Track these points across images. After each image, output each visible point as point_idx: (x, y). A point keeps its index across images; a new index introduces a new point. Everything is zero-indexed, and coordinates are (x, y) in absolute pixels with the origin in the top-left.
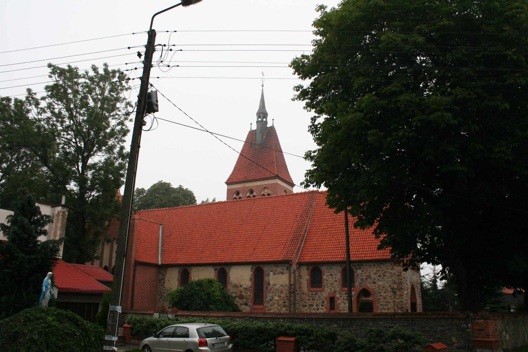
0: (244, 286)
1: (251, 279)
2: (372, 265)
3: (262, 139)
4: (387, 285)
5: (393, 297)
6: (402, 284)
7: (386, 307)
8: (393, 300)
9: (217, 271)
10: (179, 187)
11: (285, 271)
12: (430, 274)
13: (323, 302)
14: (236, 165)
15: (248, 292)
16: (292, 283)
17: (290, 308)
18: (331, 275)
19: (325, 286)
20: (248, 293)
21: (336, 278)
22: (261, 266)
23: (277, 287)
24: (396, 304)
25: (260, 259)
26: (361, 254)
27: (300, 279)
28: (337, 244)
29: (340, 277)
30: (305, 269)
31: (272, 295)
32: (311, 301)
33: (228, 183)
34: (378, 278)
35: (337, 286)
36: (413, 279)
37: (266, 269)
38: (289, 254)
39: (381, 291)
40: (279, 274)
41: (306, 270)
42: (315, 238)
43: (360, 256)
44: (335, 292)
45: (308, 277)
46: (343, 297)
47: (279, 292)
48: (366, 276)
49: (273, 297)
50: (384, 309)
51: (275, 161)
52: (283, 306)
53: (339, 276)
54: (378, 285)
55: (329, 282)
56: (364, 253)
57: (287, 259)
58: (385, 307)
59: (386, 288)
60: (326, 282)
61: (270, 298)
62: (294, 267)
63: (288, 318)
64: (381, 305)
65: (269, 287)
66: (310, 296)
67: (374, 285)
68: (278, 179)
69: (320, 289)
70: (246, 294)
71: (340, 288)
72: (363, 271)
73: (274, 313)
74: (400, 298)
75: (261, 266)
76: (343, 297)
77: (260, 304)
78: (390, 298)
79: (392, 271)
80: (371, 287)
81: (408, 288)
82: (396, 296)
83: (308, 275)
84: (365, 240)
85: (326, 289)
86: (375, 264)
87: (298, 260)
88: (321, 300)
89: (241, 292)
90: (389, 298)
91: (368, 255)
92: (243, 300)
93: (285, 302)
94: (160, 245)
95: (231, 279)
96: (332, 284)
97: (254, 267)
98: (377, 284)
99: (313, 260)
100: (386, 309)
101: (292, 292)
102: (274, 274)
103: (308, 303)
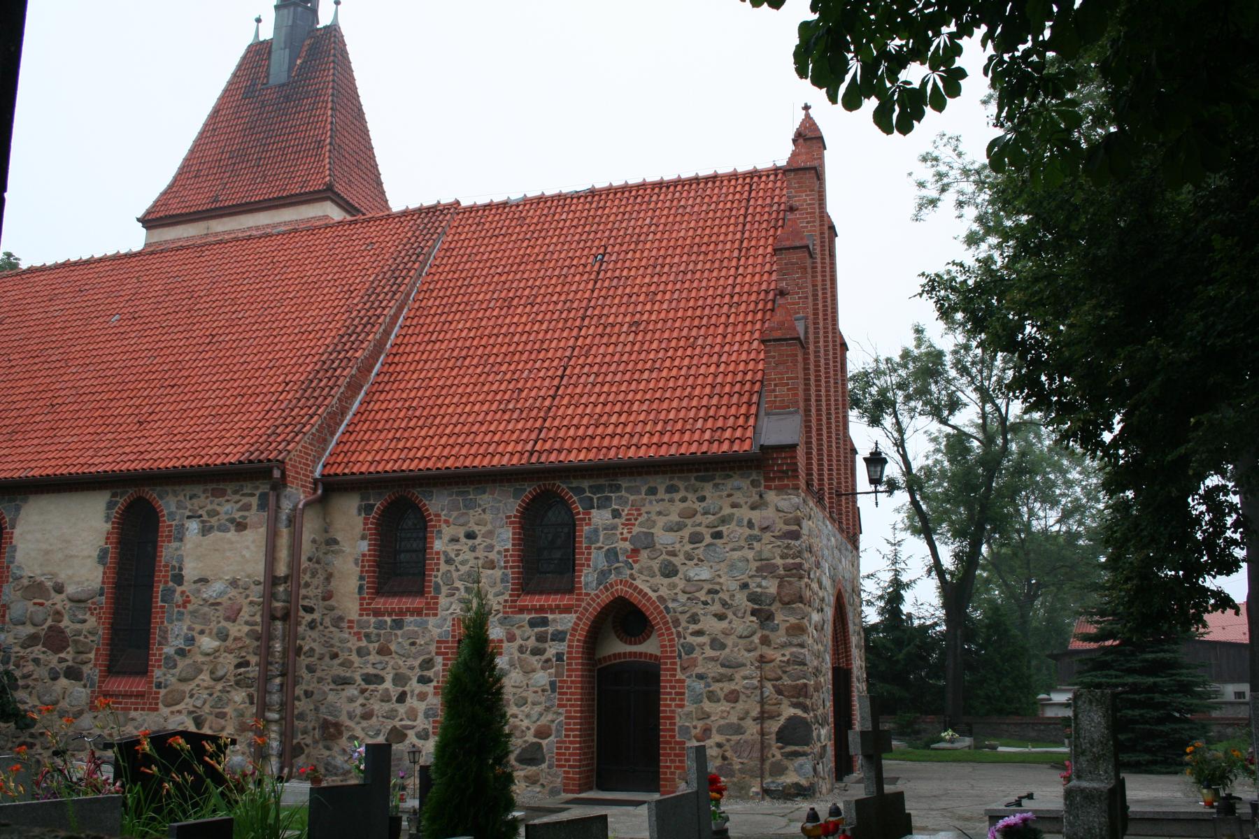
0: (70, 590)
1: (102, 558)
2: (661, 483)
3: (290, 69)
5: (756, 639)
6: (801, 577)
7: (721, 688)
8: (756, 654)
11: (254, 516)
12: (878, 575)
13: (427, 664)
14: (186, 160)
15: (87, 616)
16: (282, 570)
18: (470, 536)
19: (438, 589)
20: (84, 621)
21: (490, 548)
23: (211, 591)
24: (773, 675)
26: (612, 436)
27: (330, 556)
28: (507, 397)
29: (509, 546)
30: (354, 511)
31: (190, 629)
32: (373, 658)
34: (688, 547)
36: (840, 567)
39: (699, 609)
40: (227, 530)
43: (606, 442)
45: (364, 546)
46: (519, 642)
47: (221, 613)
48: (632, 540)
49: (193, 639)
51: (328, 140)
52: (238, 683)
53: (506, 538)
54: (689, 580)
55: (458, 570)
56: (628, 429)
58: (716, 687)
59: (726, 596)
60: (444, 567)
61: (180, 643)
62: (297, 495)
64: (700, 677)
65: (179, 589)
66: (367, 636)
67: (666, 581)
68: (333, 201)
69: (417, 602)
70: (78, 626)
71: (507, 597)
72: (616, 514)
74: (791, 644)
75: (152, 494)
76: (519, 642)
77: (137, 673)
78: (742, 641)
79: (756, 515)
80: (655, 591)
82: (772, 636)
83: (363, 538)
84: (636, 376)
85: (443, 601)
86: (675, 482)
87: (324, 466)
88: (420, 653)
89: (58, 614)
90: (736, 645)
91: (645, 440)
92: (62, 655)
93: (247, 664)
95: (19, 556)
97: (121, 501)
98: (680, 575)
101: (279, 614)
102: (206, 530)
103: (361, 667)
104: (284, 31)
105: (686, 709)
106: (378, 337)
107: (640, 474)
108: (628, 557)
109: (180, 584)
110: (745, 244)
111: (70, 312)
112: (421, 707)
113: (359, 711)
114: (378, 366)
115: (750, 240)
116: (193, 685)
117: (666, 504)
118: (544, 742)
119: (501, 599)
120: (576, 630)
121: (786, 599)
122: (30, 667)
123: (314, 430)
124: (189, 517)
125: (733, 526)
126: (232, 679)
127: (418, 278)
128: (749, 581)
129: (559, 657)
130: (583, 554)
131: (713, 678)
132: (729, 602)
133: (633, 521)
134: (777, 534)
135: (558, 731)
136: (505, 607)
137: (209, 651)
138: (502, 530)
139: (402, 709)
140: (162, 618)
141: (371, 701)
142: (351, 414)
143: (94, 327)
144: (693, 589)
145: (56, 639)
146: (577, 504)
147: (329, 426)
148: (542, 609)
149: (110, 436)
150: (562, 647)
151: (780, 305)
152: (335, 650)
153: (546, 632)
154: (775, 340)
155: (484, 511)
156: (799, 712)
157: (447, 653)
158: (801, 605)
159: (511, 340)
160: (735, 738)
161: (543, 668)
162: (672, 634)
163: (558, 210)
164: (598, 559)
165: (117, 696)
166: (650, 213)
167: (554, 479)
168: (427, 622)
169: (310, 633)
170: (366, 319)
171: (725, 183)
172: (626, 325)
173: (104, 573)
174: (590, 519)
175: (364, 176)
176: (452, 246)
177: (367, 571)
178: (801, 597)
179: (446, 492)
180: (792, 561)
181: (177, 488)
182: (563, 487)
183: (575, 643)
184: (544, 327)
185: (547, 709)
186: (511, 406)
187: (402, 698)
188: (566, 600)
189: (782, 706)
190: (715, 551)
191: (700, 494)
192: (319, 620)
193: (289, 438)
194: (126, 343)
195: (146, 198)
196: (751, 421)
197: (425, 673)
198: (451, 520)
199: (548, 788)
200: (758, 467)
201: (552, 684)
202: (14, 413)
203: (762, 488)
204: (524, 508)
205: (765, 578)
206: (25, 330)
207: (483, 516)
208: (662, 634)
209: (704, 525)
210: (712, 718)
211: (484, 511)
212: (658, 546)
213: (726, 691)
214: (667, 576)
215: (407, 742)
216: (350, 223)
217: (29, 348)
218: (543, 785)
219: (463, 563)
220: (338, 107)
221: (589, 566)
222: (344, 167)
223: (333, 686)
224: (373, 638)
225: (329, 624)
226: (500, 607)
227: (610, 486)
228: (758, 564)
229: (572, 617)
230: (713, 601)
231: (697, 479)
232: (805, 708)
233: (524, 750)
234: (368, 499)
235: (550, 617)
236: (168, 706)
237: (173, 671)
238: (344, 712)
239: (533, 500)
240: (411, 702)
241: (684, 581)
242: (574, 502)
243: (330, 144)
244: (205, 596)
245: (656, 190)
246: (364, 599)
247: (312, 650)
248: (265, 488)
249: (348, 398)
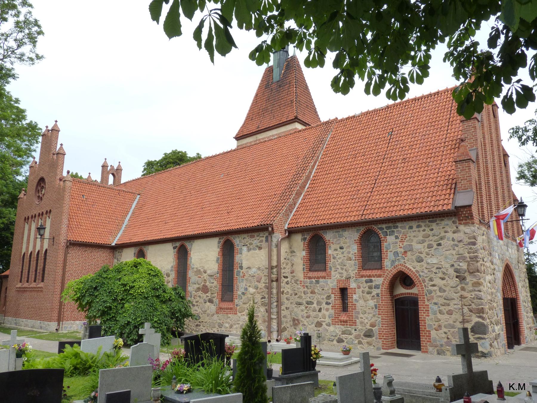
0: (209, 272)
1: (217, 261)
2: (414, 224)
3: (280, 75)
5: (459, 288)
7: (445, 309)
8: (459, 294)
11: (264, 244)
13: (329, 297)
14: (248, 114)
15: (214, 281)
18: (341, 248)
19: (331, 268)
20: (213, 283)
24: (467, 304)
29: (356, 252)
30: (300, 240)
31: (246, 285)
32: (309, 295)
34: (427, 250)
36: (507, 253)
39: (433, 275)
44: (348, 278)
45: (304, 253)
46: (362, 289)
52: (262, 304)
53: (354, 249)
58: (442, 308)
60: (332, 260)
62: (278, 236)
64: (435, 304)
65: (242, 271)
66: (307, 287)
68: (298, 122)
70: (211, 284)
71: (356, 272)
72: (397, 237)
74: (475, 291)
75: (231, 238)
76: (362, 289)
79: (456, 236)
80: (414, 268)
81: (494, 269)
82: (466, 287)
83: (304, 250)
86: (420, 223)
95: (193, 261)
97: (222, 241)
98: (424, 261)
99: (311, 223)
100: (445, 312)
101: (274, 280)
102: (249, 250)
104: (277, 61)
105: (430, 317)
106: (307, 174)
107: (405, 221)
108: (402, 255)
109: (242, 269)
110: (451, 120)
111: (209, 174)
112: (327, 314)
113: (305, 315)
114: (308, 185)
115: (453, 117)
117: (417, 233)
118: (374, 329)
120: (384, 284)
121: (471, 271)
122: (198, 299)
123: (283, 212)
124: (243, 246)
125: (445, 240)
126: (260, 303)
127: (322, 150)
128: (454, 264)
129: (378, 295)
130: (385, 254)
131: (441, 304)
132: (446, 272)
133: (404, 240)
134: (465, 243)
135: (379, 324)
136: (356, 275)
137: (252, 293)
138: (353, 245)
139: (320, 314)
140: (237, 281)
141: (309, 311)
142: (298, 204)
143: (216, 179)
144: (430, 267)
145: (205, 289)
146: (381, 234)
147: (290, 210)
148: (370, 276)
149: (219, 218)
150: (379, 291)
151: (462, 146)
152: (296, 292)
154: (460, 161)
155: (346, 238)
156: (480, 320)
157: (335, 293)
158: (478, 273)
159: (355, 170)
160: (452, 330)
161: (372, 299)
162: (422, 286)
163: (375, 116)
165: (224, 309)
166: (411, 112)
167: (371, 224)
168: (327, 281)
169: (287, 285)
170: (303, 168)
171: (443, 94)
172: (401, 160)
173: (218, 266)
174: (386, 240)
175: (310, 110)
176: (335, 136)
177: (306, 263)
178: (478, 270)
179: (332, 232)
180: (473, 255)
181: (239, 235)
182: (375, 227)
183: (384, 289)
184: (368, 164)
185: (374, 316)
186: (355, 197)
187: (320, 310)
188: (379, 272)
189: (472, 317)
190: (438, 251)
191: (431, 228)
192: (290, 281)
193: (274, 216)
194: (225, 184)
195: (235, 131)
196: (452, 196)
197: (328, 301)
198: (334, 242)
199: (376, 347)
200: (455, 215)
201: (375, 305)
202: (191, 212)
203: (457, 224)
204: (361, 237)
206: (195, 182)
207: (346, 240)
208: (418, 286)
209: (433, 240)
210: (442, 321)
211: (346, 238)
212: (414, 250)
213: (447, 310)
214: (419, 262)
215: (322, 327)
216: (306, 129)
217: (196, 188)
218: (374, 346)
219: (339, 258)
220: (298, 86)
221: (387, 258)
222: (301, 108)
223: (296, 305)
224: (309, 287)
225: (293, 282)
226: (354, 275)
227: (394, 226)
228: (458, 256)
230: (439, 272)
231: (429, 221)
232: (483, 318)
233: (366, 332)
234: (304, 236)
235: (373, 279)
236: (240, 313)
238: (300, 315)
239: (365, 233)
240: (323, 311)
241: (426, 264)
242: (380, 233)
243: (296, 101)
244: (250, 273)
245: (414, 102)
246: (305, 273)
247: (288, 292)
248: (267, 234)
249: (296, 199)
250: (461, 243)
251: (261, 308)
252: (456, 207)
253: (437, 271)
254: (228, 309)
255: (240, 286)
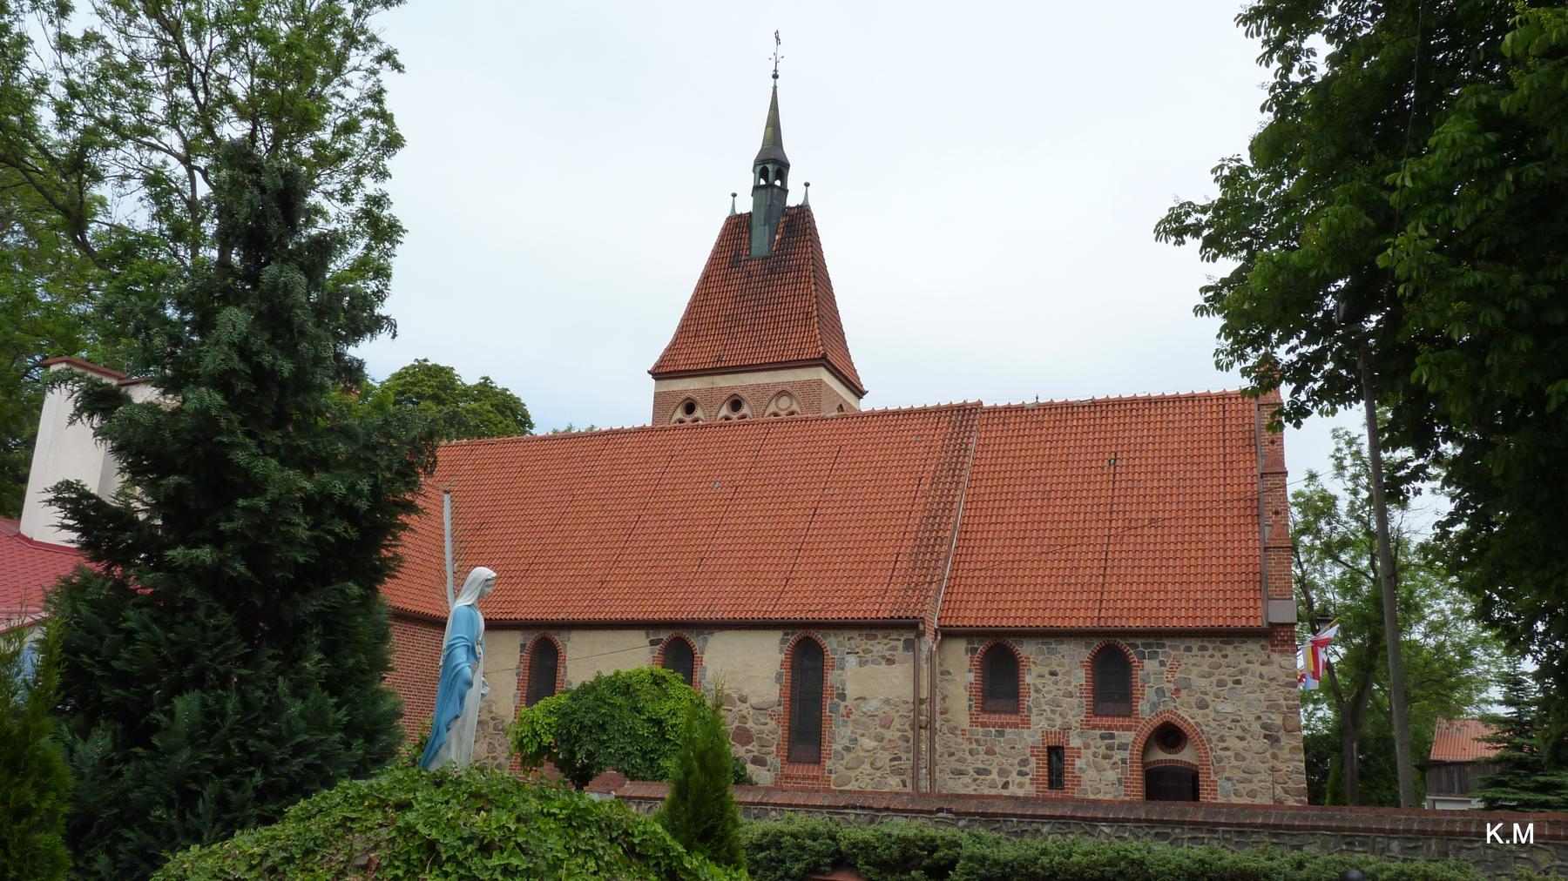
0: (753, 700)
1: (778, 678)
2: (1195, 644)
4: (1248, 716)
5: (1268, 755)
9: (658, 647)
10: (480, 384)
11: (900, 653)
13: (1024, 762)
14: (684, 320)
15: (768, 720)
17: (916, 780)
18: (1053, 674)
19: (1029, 709)
20: (766, 724)
21: (1069, 683)
22: (818, 635)
23: (872, 706)
24: (1281, 781)
25: (814, 612)
30: (963, 652)
31: (853, 732)
32: (982, 756)
33: (659, 374)
35: (1074, 710)
37: (832, 643)
38: (911, 597)
39: (1225, 732)
41: (967, 654)
42: (987, 551)
44: (1066, 729)
45: (971, 677)
46: (1093, 749)
49: (856, 740)
50: (1236, 793)
52: (892, 772)
53: (1080, 677)
57: (908, 614)
58: (1239, 786)
60: (1033, 695)
61: (846, 742)
63: (1138, 820)
64: (1228, 779)
65: (843, 704)
66: (977, 741)
69: (1013, 719)
72: (1162, 664)
73: (861, 793)
74: (1294, 760)
75: (818, 635)
76: (1093, 749)
79: (1265, 670)
82: (1280, 754)
83: (970, 671)
85: (1034, 718)
88: (1018, 754)
90: (1253, 758)
93: (899, 759)
94: (449, 556)
96: (1055, 703)
97: (792, 639)
101: (923, 725)
102: (862, 663)
116: (857, 772)
119: (1078, 719)
121: (1289, 729)
124: (848, 653)
125: (1248, 676)
128: (1262, 715)
129: (1124, 761)
138: (1077, 671)
148: (1109, 728)
150: (1126, 754)
152: (952, 750)
153: (1114, 744)
155: (1063, 657)
164: (1150, 694)
165: (797, 778)
182: (1122, 642)
188: (1127, 722)
195: (653, 358)
197: (1022, 769)
205: (1273, 713)
211: (1063, 657)
223: (952, 776)
226: (1078, 725)
227: (1157, 644)
228: (1268, 703)
229: (1133, 734)
231: (1222, 642)
235: (1116, 733)
237: (841, 762)
250: (1275, 683)
251: (889, 779)
252: (1270, 624)
253: (1233, 726)
254: (808, 779)
255: (838, 734)
